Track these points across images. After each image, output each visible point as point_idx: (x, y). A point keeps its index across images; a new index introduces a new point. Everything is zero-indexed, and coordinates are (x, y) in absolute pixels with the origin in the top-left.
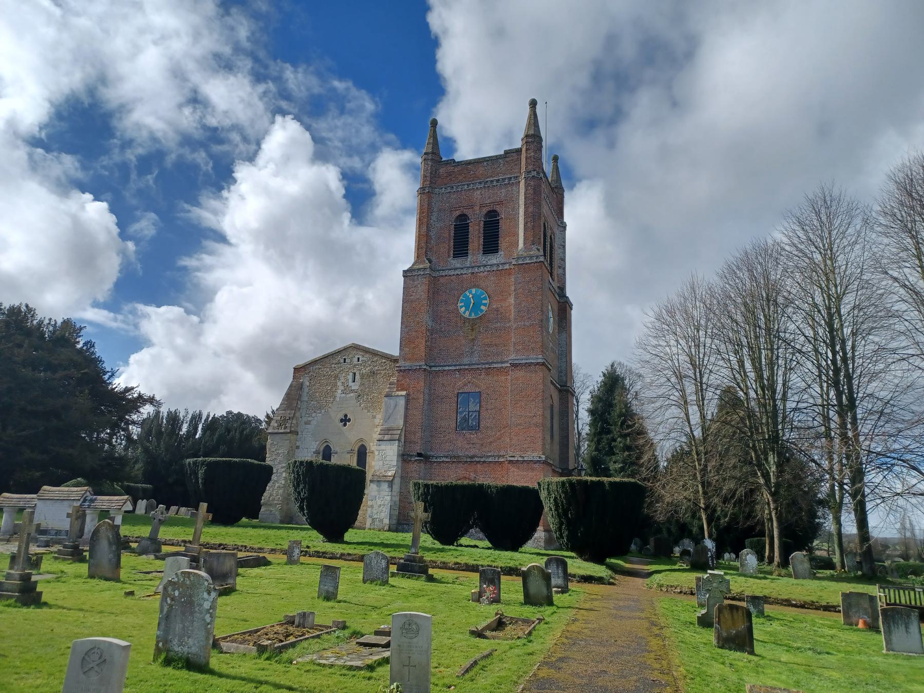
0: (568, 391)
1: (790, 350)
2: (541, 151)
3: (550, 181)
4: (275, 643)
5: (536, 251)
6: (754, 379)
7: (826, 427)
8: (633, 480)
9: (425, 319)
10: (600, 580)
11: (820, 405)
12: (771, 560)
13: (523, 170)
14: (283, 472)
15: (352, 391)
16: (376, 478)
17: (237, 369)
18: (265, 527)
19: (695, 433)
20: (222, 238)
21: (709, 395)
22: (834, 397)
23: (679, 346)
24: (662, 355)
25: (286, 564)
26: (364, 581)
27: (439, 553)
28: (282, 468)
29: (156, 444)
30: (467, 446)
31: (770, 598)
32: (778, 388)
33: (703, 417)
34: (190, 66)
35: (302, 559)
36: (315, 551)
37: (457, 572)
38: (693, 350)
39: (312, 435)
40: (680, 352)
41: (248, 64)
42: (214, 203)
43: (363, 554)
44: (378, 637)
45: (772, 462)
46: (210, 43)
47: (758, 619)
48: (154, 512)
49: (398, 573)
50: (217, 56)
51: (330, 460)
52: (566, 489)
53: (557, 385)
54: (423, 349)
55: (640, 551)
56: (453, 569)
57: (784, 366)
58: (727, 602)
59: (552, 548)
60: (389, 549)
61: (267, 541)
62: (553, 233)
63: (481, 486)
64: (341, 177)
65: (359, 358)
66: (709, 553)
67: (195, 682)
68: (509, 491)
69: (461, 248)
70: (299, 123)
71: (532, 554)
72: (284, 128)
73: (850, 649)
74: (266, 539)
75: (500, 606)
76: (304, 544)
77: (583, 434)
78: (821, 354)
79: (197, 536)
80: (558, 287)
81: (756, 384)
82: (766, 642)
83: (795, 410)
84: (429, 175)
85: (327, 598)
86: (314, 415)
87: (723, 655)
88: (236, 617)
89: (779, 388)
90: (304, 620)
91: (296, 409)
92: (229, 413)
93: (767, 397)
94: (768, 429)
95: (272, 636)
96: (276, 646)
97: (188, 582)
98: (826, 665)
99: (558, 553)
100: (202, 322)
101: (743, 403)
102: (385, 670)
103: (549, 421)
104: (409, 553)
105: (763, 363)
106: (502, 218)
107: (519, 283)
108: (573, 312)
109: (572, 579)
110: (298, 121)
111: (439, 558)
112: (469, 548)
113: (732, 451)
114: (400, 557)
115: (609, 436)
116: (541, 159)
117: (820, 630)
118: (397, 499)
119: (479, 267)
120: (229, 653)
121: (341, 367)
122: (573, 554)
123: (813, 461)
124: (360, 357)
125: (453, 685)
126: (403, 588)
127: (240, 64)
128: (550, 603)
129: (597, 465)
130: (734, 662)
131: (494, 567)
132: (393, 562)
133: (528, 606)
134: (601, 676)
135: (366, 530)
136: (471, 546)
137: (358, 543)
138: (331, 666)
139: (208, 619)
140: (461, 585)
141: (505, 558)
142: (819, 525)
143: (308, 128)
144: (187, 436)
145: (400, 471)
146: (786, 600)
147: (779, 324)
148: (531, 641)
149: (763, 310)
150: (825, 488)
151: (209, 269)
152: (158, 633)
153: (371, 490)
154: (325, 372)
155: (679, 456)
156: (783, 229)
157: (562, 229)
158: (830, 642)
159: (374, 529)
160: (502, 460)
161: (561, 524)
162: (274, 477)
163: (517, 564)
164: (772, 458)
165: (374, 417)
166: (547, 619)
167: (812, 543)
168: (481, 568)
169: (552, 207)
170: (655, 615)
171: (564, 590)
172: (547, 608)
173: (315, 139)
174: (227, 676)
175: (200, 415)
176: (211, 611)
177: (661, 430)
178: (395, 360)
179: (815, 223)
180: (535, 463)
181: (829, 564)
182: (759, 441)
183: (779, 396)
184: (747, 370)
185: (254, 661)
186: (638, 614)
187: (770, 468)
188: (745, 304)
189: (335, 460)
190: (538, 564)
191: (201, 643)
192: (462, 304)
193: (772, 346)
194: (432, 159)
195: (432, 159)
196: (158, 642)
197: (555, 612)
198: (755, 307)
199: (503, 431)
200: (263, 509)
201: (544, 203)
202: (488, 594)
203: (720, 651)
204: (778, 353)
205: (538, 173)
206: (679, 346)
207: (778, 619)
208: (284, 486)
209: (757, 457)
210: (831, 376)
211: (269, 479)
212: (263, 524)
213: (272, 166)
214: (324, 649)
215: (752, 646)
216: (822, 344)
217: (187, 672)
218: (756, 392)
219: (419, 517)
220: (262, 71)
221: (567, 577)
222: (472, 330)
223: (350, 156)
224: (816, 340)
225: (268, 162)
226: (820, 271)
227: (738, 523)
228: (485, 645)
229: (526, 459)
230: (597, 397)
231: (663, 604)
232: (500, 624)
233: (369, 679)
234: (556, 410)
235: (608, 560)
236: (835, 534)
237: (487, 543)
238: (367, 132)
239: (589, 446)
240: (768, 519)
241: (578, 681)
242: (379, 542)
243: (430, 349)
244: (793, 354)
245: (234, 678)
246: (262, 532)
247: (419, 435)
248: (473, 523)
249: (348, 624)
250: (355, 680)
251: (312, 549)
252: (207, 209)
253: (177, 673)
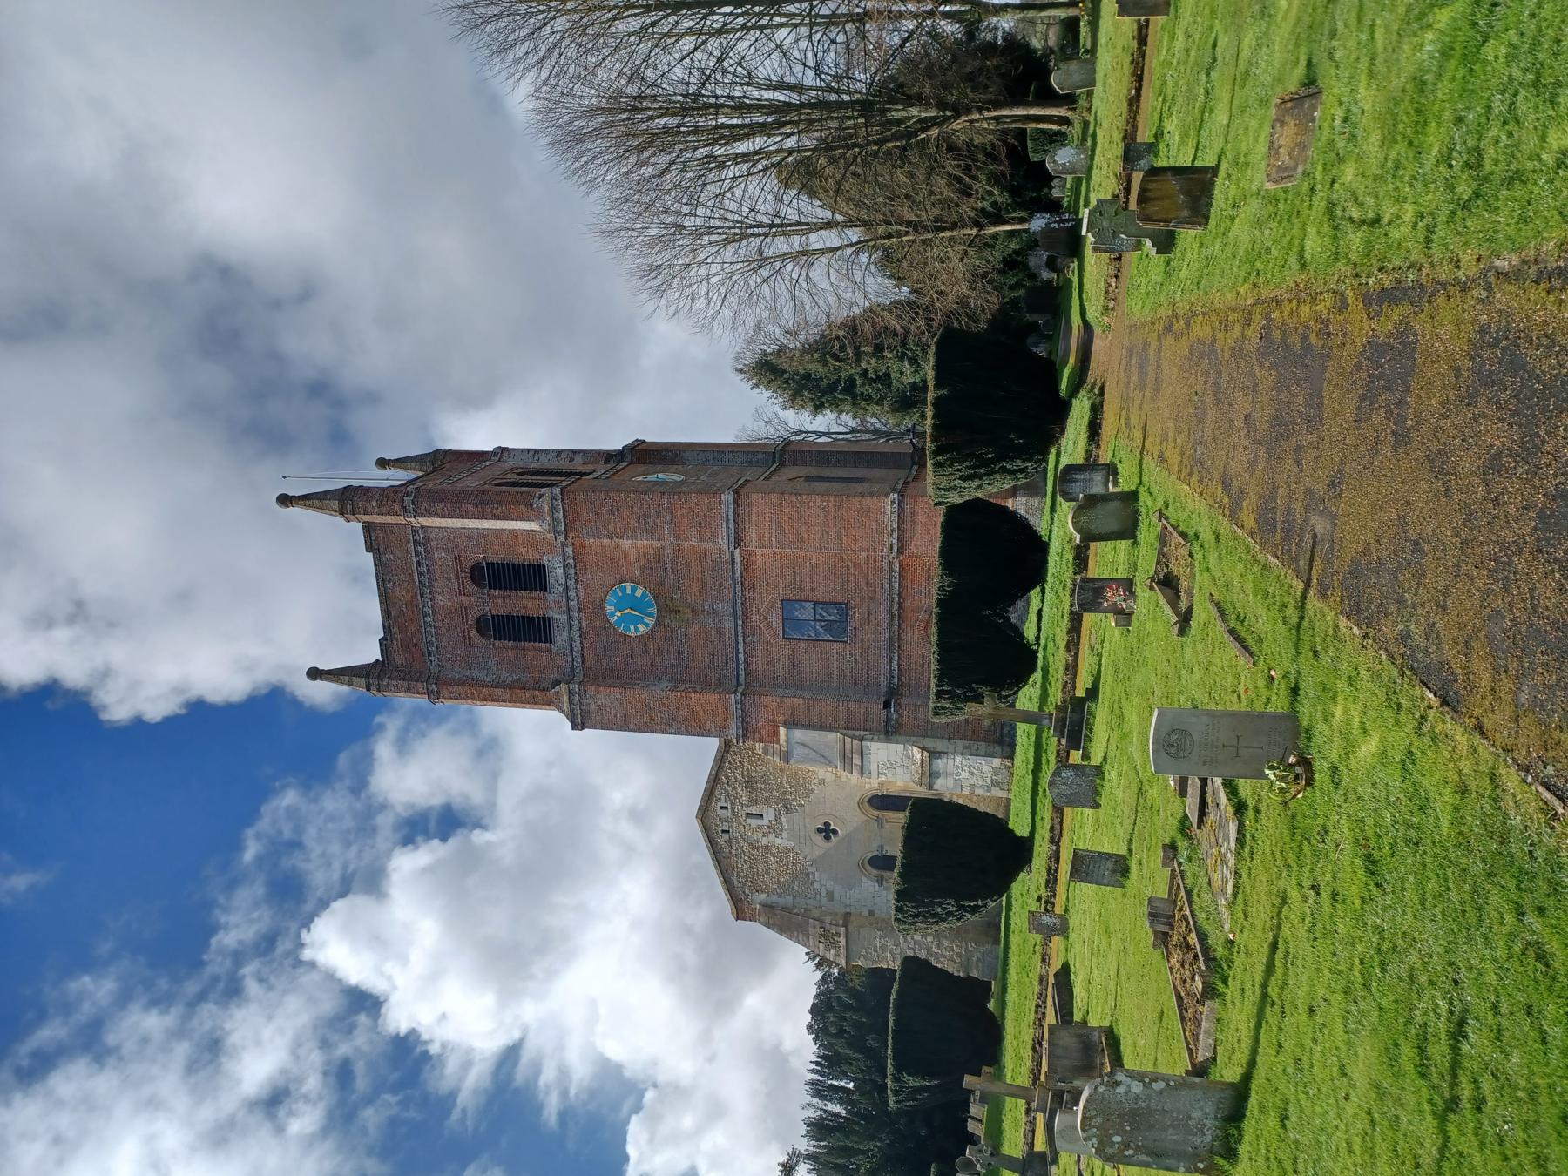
0: (783, 451)
1: (719, 76)
2: (368, 489)
3: (421, 474)
4: (1199, 968)
5: (545, 500)
6: (765, 138)
7: (847, 21)
8: (933, 347)
9: (655, 694)
10: (1096, 410)
11: (811, 29)
12: (1064, 121)
13: (400, 519)
14: (912, 938)
15: (778, 819)
16: (925, 780)
17: (738, 1023)
18: (1005, 971)
19: (855, 239)
20: (511, 1054)
21: (791, 214)
22: (797, 5)
23: (709, 261)
24: (723, 290)
25: (1067, 938)
26: (1097, 806)
27: (1050, 677)
28: (906, 941)
29: (861, 1157)
30: (874, 623)
31: (1126, 130)
32: (782, 98)
33: (828, 225)
34: (207, 1114)
35: (1059, 910)
36: (1047, 886)
37: (1081, 647)
38: (716, 238)
39: (850, 889)
40: (719, 259)
41: (208, 1009)
42: (451, 1067)
43: (1051, 805)
44: (1190, 790)
45: (903, 113)
46: (169, 1082)
47: (1161, 153)
48: (979, 1165)
49: (1084, 748)
50: (191, 1068)
51: (894, 859)
52: (946, 460)
53: (772, 469)
54: (708, 697)
55: (1049, 337)
56: (1077, 654)
57: (745, 87)
58: (1133, 205)
59: (1042, 484)
60: (1044, 762)
61: (1028, 969)
62: (512, 470)
63: (941, 603)
64: (410, 847)
65: (722, 808)
66: (1052, 226)
67: (1262, 1107)
68: (949, 555)
69: (536, 630)
70: (316, 919)
71: (1052, 519)
72: (323, 944)
73: (1207, 10)
74: (1025, 969)
75: (1138, 581)
76: (1034, 906)
77: (854, 425)
78: (725, 24)
79: (1018, 1092)
80: (605, 463)
81: (775, 135)
82: (1198, 145)
83: (818, 74)
84: (405, 684)
85: (1125, 871)
86: (817, 885)
87: (1219, 217)
88: (1156, 1030)
89: (780, 96)
90: (1162, 916)
91: (806, 914)
92: (810, 1028)
93: (796, 118)
94: (849, 118)
95: (1187, 972)
96: (1203, 968)
97: (1099, 1120)
98: (1233, 51)
99: (1050, 474)
100: (655, 1086)
101: (807, 157)
102: (1245, 787)
103: (833, 484)
104: (1049, 729)
105: (739, 121)
106: (485, 557)
107: (597, 529)
108: (648, 439)
109: (1093, 457)
110: (311, 920)
111: (1058, 676)
112: (1043, 625)
113: (885, 179)
114: (1056, 742)
115: (859, 381)
116: (383, 489)
117: (1177, 55)
118: (959, 743)
119: (568, 598)
120: (1215, 1048)
121: (736, 839)
122: (1053, 451)
123: (902, 45)
124: (719, 805)
125: (1269, 672)
126: (1108, 740)
127: (207, 1026)
128: (1133, 496)
129: (908, 401)
130: (1231, 201)
131: (1074, 585)
132: (1064, 755)
133: (1138, 533)
134: (1255, 425)
135: (1012, 797)
136: (1039, 621)
137: (1034, 813)
138: (1237, 874)
139: (1161, 1085)
140: (1103, 641)
141: (1058, 564)
142: (1009, 38)
143: (324, 904)
144: (849, 1104)
145: (914, 739)
146: (1130, 105)
147: (675, 94)
148: (1196, 534)
149: (650, 118)
150: (949, 28)
151: (564, 1073)
152: (1182, 1169)
153: (945, 788)
154: (745, 866)
155: (890, 262)
156: (512, 80)
157: (506, 454)
158: (1197, 40)
159: (1010, 784)
160: (897, 565)
161: (1003, 470)
162: (922, 954)
163: (1068, 547)
164: (897, 113)
165: (822, 781)
166: (1160, 504)
167: (1035, 51)
168: (1076, 608)
169: (467, 470)
170: (1154, 324)
171: (1111, 470)
172: (1141, 502)
173: (343, 894)
174: (1254, 1052)
175: (812, 1083)
176: (1147, 1080)
177: (849, 295)
178: (727, 745)
179: (502, 24)
180: (903, 510)
181: (1071, 26)
182: (868, 135)
183: (795, 98)
184: (752, 149)
185: (1229, 1005)
186: (1152, 352)
187: (913, 117)
188: (640, 149)
189: (895, 849)
190: (1070, 517)
191: (1199, 1097)
192: (632, 628)
193: (711, 106)
194: (379, 678)
195: (379, 678)
196: (1197, 1170)
197: (1148, 489)
198: (645, 132)
199: (849, 563)
200: (975, 974)
201: (459, 486)
202: (1117, 599)
203: (1212, 222)
204: (723, 97)
205: (408, 494)
206: (709, 261)
207: (1161, 121)
208: (937, 935)
209: (895, 137)
210: (762, 8)
211: (926, 963)
212: (1000, 974)
213: (389, 967)
214: (1209, 884)
215: (1204, 169)
216: (708, 22)
217: (1246, 1119)
218: (788, 135)
219: (992, 712)
220: (221, 985)
221: (1090, 465)
222: (676, 612)
223: (374, 830)
224: (700, 32)
225: (381, 974)
226: (585, 20)
227: (1003, 174)
228: (1202, 613)
229: (895, 526)
230: (793, 399)
231: (1136, 307)
232: (1168, 583)
233: (1258, 811)
234: (812, 471)
235: (1063, 394)
236: (1021, 15)
237: (1034, 594)
238: (335, 801)
239: (874, 415)
240: (998, 123)
241: (1261, 465)
242: (1031, 776)
243: (709, 686)
244: (725, 71)
245: (1256, 1041)
246: (1013, 976)
247: (853, 706)
248: (1002, 617)
249: (1167, 841)
250: (1259, 835)
251: (1044, 892)
252: (462, 1079)
253: (1248, 1137)
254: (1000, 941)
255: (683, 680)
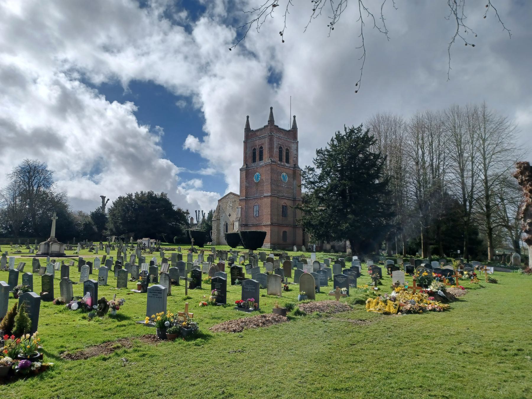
9: (245, 183)
69: (254, 160)
254: (487, 255)
255: (247, 188)
